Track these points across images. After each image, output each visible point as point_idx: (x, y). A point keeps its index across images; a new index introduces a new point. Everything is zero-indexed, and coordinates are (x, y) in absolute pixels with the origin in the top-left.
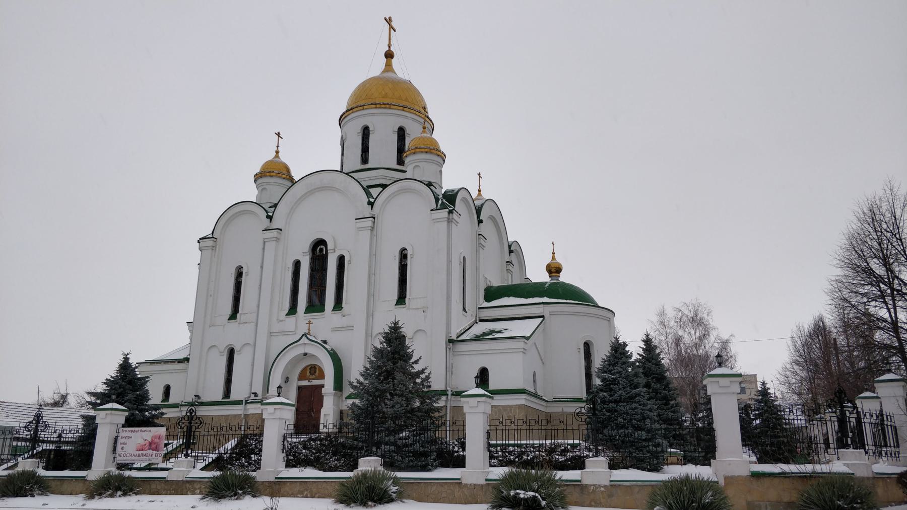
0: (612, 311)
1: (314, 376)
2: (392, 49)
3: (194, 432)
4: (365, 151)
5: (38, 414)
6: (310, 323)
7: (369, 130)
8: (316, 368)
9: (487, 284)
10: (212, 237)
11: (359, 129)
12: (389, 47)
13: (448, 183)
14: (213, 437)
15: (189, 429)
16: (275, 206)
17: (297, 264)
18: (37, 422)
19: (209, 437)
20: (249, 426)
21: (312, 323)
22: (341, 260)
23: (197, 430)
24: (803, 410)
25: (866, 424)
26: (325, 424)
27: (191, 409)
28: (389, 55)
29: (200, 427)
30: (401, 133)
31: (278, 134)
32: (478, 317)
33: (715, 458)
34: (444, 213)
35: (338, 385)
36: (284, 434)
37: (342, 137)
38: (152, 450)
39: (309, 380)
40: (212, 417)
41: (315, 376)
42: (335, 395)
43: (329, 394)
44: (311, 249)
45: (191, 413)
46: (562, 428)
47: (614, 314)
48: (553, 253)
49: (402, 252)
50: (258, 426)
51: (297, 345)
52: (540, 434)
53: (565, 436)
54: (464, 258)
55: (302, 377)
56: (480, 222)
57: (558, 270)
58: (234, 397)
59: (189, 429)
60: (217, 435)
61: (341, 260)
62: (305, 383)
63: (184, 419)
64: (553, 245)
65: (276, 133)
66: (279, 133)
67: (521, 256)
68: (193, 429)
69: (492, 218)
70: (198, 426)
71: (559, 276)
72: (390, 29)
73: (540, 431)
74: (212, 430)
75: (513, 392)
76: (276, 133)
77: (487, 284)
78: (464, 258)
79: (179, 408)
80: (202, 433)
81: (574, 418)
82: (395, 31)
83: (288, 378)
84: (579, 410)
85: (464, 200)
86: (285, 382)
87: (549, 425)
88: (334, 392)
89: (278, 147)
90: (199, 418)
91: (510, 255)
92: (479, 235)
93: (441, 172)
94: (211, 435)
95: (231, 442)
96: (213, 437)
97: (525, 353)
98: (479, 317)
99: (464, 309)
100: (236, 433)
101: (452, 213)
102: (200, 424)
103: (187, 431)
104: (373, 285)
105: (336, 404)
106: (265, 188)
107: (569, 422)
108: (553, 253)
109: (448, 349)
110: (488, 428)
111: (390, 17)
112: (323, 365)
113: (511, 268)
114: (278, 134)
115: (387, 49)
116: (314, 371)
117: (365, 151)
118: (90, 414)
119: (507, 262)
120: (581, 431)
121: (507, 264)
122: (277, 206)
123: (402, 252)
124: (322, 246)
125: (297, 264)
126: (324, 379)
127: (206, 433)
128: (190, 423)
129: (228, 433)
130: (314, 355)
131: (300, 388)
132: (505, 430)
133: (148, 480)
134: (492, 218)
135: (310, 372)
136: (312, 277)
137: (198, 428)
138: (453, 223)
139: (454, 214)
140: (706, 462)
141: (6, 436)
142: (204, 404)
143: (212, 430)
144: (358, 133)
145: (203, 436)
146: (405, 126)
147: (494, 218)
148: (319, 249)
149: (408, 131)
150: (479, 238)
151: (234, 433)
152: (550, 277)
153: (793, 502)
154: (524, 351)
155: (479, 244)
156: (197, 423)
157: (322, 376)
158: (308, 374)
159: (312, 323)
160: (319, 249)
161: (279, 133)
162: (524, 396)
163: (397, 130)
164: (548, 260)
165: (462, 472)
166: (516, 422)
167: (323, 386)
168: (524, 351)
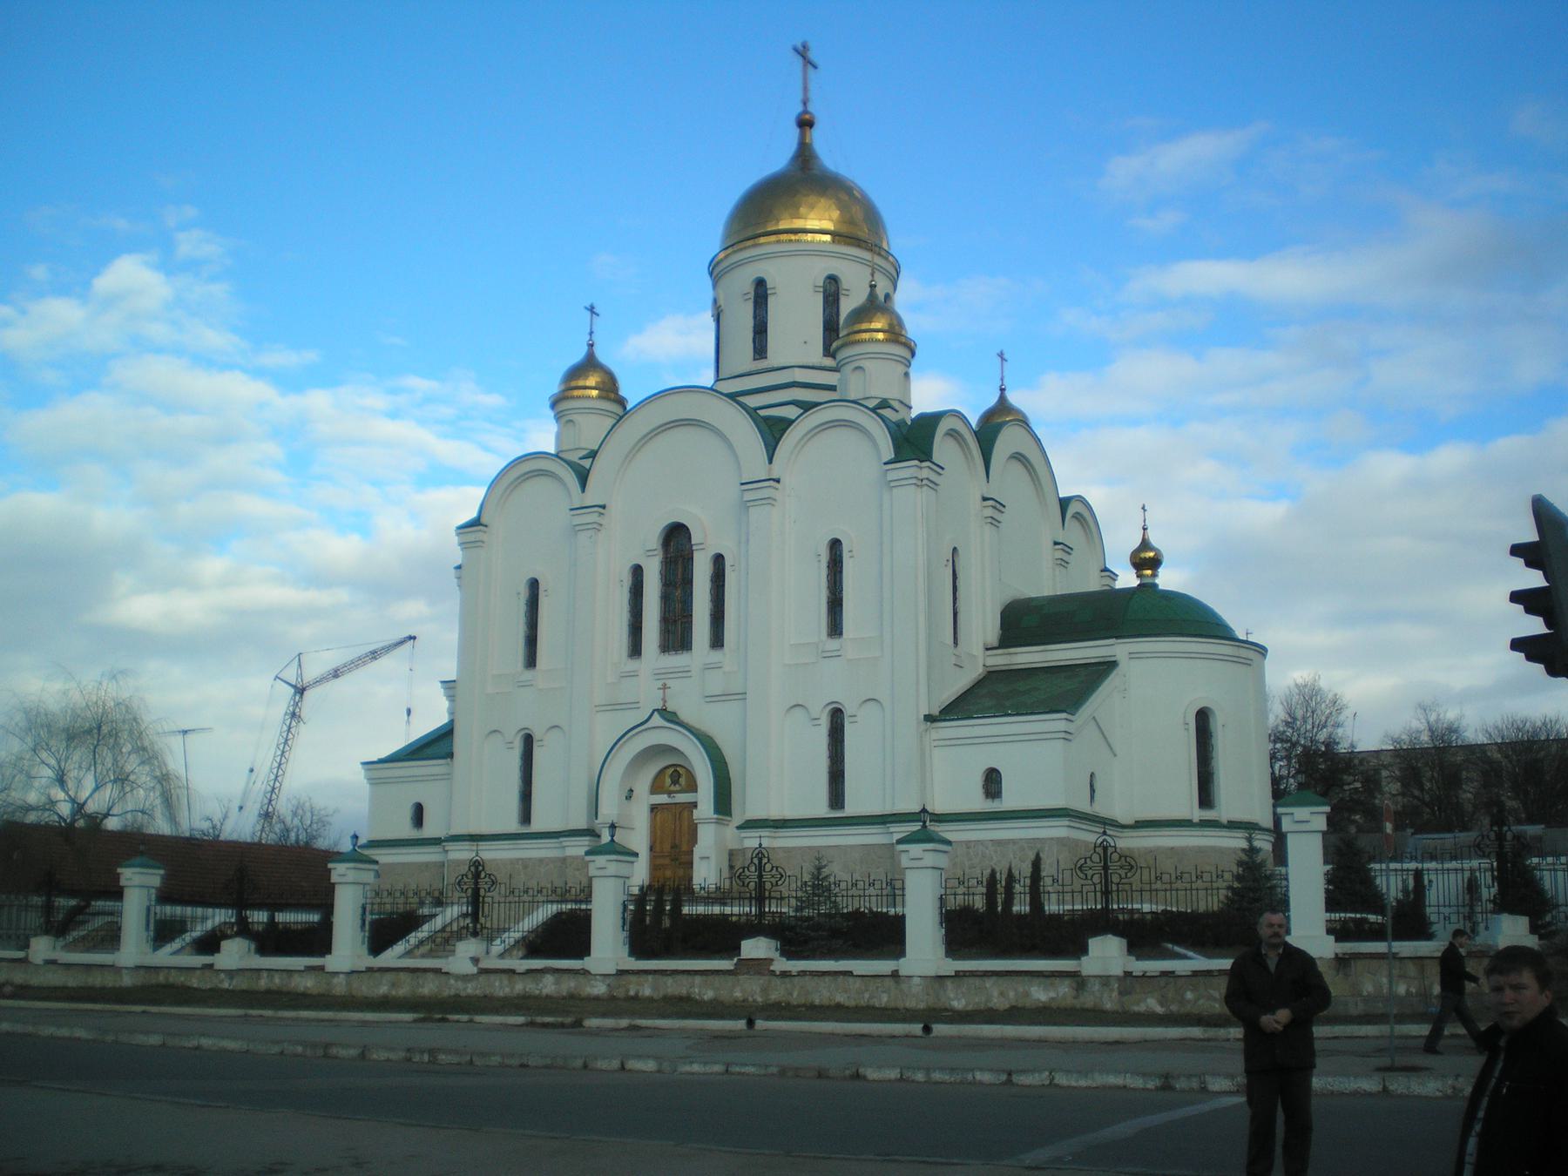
1: (677, 788)
2: (810, 108)
3: (483, 897)
4: (760, 330)
5: (475, 862)
6: (664, 687)
7: (766, 290)
10: (476, 523)
11: (749, 288)
14: (527, 904)
15: (476, 892)
16: (593, 455)
17: (637, 571)
18: (477, 876)
19: (850, 899)
20: (1220, 873)
22: (719, 560)
23: (488, 894)
24: (1414, 854)
25: (897, 897)
26: (703, 885)
27: (1104, 840)
28: (805, 123)
29: (492, 889)
30: (832, 291)
31: (592, 309)
36: (942, 895)
37: (715, 301)
39: (669, 793)
40: (1153, 853)
41: (680, 785)
43: (707, 821)
44: (661, 541)
45: (477, 868)
50: (1220, 873)
53: (1130, 899)
55: (656, 788)
57: (1155, 563)
59: (476, 892)
60: (1191, 889)
61: (719, 560)
62: (662, 799)
63: (466, 876)
64: (1145, 510)
68: (482, 892)
69: (1019, 457)
70: (489, 888)
72: (805, 66)
73: (1168, 893)
74: (1159, 882)
80: (496, 900)
81: (1074, 874)
83: (631, 791)
86: (626, 798)
87: (962, 887)
88: (715, 816)
89: (591, 333)
90: (1126, 857)
96: (527, 904)
97: (512, 748)
100: (1193, 887)
102: (492, 886)
103: (755, 889)
106: (571, 421)
107: (1067, 881)
110: (943, 892)
112: (690, 763)
114: (592, 309)
115: (800, 109)
116: (676, 776)
117: (760, 330)
120: (1084, 893)
122: (595, 455)
125: (637, 571)
126: (696, 792)
127: (503, 900)
128: (476, 883)
129: (850, 893)
130: (675, 749)
131: (654, 809)
136: (666, 598)
137: (489, 891)
141: (383, 901)
143: (1159, 882)
147: (1020, 454)
148: (676, 538)
151: (531, 899)
152: (1138, 577)
154: (1067, 736)
156: (486, 883)
157: (692, 787)
158: (668, 781)
160: (676, 538)
162: (1065, 822)
167: (694, 805)
168: (1067, 736)
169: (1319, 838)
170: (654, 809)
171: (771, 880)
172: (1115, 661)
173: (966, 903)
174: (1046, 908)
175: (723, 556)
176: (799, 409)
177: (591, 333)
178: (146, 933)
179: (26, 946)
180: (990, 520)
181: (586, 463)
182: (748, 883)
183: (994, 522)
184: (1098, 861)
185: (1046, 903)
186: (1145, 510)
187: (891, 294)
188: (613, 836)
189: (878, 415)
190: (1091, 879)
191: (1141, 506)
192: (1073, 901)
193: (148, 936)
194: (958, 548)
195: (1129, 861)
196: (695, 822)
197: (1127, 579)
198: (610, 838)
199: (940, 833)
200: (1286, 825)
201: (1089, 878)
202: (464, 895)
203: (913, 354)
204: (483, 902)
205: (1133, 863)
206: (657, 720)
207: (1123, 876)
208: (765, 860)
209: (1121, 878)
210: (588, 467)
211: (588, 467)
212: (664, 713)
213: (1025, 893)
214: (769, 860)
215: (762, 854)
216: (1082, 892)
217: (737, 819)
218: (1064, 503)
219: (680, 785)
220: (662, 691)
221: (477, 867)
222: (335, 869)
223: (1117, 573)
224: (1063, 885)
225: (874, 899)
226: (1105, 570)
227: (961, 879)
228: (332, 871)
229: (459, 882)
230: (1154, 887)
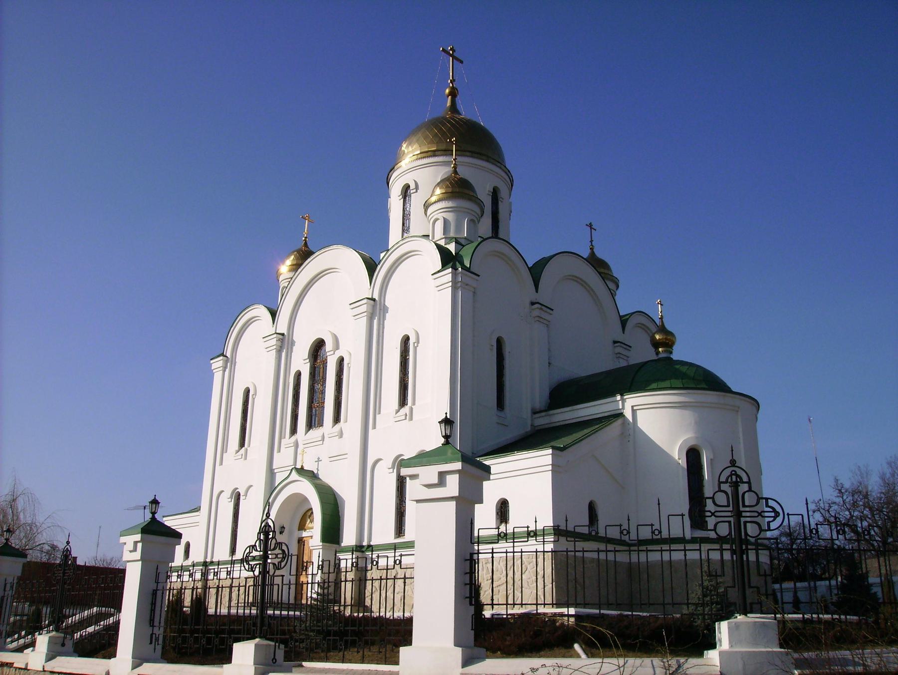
23: (278, 572)
29: (283, 564)
31: (590, 226)
33: (481, 502)
65: (587, 225)
66: (590, 224)
75: (318, 387)
76: (587, 225)
84: (745, 479)
89: (591, 241)
94: (372, 580)
104: (320, 252)
114: (590, 226)
118: (549, 571)
129: (392, 574)
140: (117, 576)
145: (371, 581)
153: (444, 118)
161: (590, 224)
165: (728, 623)
171: (759, 519)
173: (107, 612)
177: (591, 241)
180: (537, 319)
183: (541, 320)
188: (153, 513)
190: (715, 530)
192: (662, 563)
198: (150, 516)
199: (177, 530)
202: (251, 574)
204: (272, 585)
205: (778, 509)
208: (743, 488)
209: (761, 530)
214: (750, 488)
215: (738, 476)
225: (377, 584)
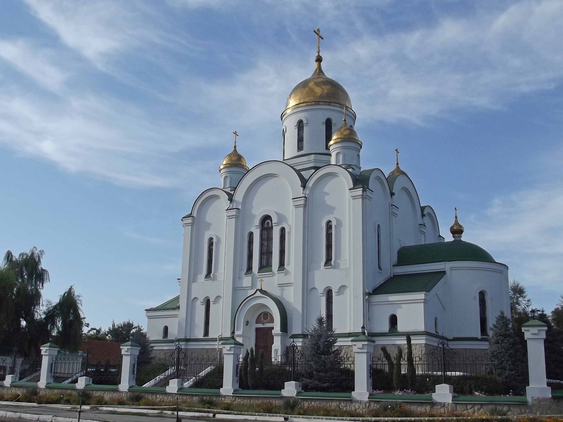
0: (505, 265)
1: (266, 321)
8: (267, 314)
9: (400, 245)
12: (318, 53)
13: (365, 167)
17: (251, 234)
21: (263, 281)
22: (283, 230)
31: (235, 133)
32: (392, 273)
34: (359, 192)
35: (284, 327)
36: (371, 364)
38: (490, 391)
42: (281, 336)
43: (277, 335)
44: (260, 223)
46: (380, 363)
47: (508, 267)
48: (456, 217)
49: (328, 223)
51: (253, 298)
52: (423, 366)
54: (379, 226)
56: (392, 194)
58: (211, 335)
62: (260, 326)
65: (233, 133)
66: (236, 132)
67: (435, 219)
69: (406, 190)
71: (461, 237)
77: (400, 245)
78: (379, 226)
79: (175, 343)
81: (429, 357)
82: (322, 39)
85: (378, 179)
86: (246, 325)
87: (379, 361)
91: (422, 219)
92: (392, 205)
93: (359, 155)
95: (204, 371)
98: (393, 273)
99: (380, 268)
100: (196, 363)
101: (366, 191)
105: (282, 343)
108: (456, 217)
109: (365, 300)
110: (371, 363)
111: (315, 30)
112: (271, 311)
113: (423, 230)
115: (317, 54)
116: (266, 316)
119: (420, 225)
121: (420, 226)
123: (328, 223)
124: (269, 221)
131: (257, 330)
132: (382, 364)
133: (226, 411)
134: (406, 190)
135: (263, 318)
138: (367, 199)
139: (367, 191)
142: (191, 340)
144: (295, 126)
146: (331, 118)
147: (406, 188)
149: (334, 122)
150: (392, 208)
152: (453, 237)
155: (392, 213)
157: (272, 321)
159: (263, 281)
161: (236, 132)
163: (325, 122)
164: (452, 223)
166: (381, 359)
167: (273, 328)
169: (543, 342)
170: (257, 330)
172: (445, 271)
174: (417, 373)
175: (284, 228)
176: (242, 341)
178: (50, 374)
179: (481, 338)
181: (232, 192)
182: (437, 357)
184: (296, 358)
185: (417, 370)
186: (456, 210)
187: (353, 125)
189: (347, 171)
191: (455, 208)
193: (51, 375)
194: (380, 225)
195: (455, 352)
196: (273, 335)
197: (449, 238)
200: (448, 344)
201: (436, 357)
203: (361, 148)
206: (258, 294)
207: (299, 358)
210: (233, 194)
211: (233, 194)
212: (261, 291)
213: (424, 364)
216: (433, 364)
217: (290, 335)
218: (423, 209)
219: (267, 320)
220: (260, 282)
221: (179, 349)
222: (123, 349)
223: (445, 238)
224: (382, 361)
226: (440, 236)
227: (379, 357)
228: (122, 350)
229: (172, 355)
230: (465, 362)
